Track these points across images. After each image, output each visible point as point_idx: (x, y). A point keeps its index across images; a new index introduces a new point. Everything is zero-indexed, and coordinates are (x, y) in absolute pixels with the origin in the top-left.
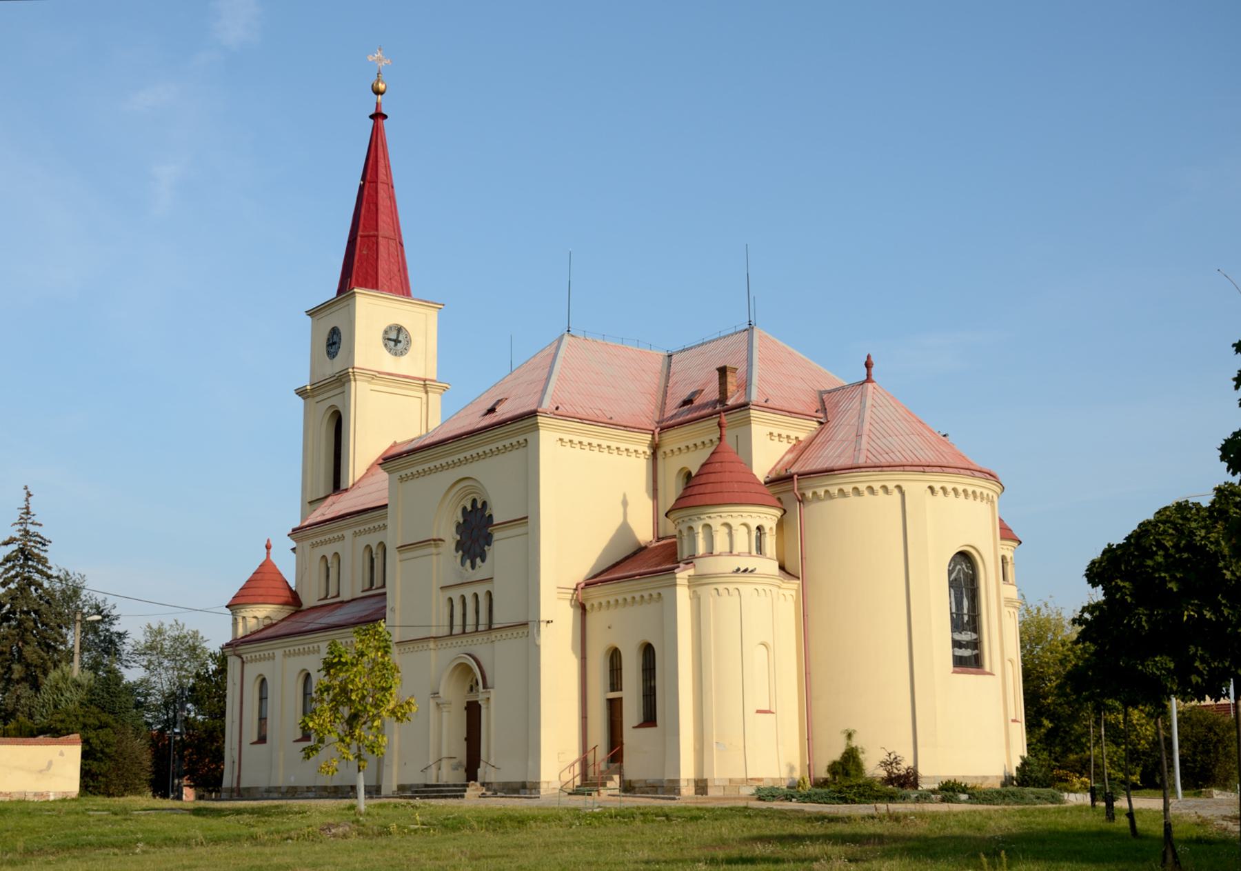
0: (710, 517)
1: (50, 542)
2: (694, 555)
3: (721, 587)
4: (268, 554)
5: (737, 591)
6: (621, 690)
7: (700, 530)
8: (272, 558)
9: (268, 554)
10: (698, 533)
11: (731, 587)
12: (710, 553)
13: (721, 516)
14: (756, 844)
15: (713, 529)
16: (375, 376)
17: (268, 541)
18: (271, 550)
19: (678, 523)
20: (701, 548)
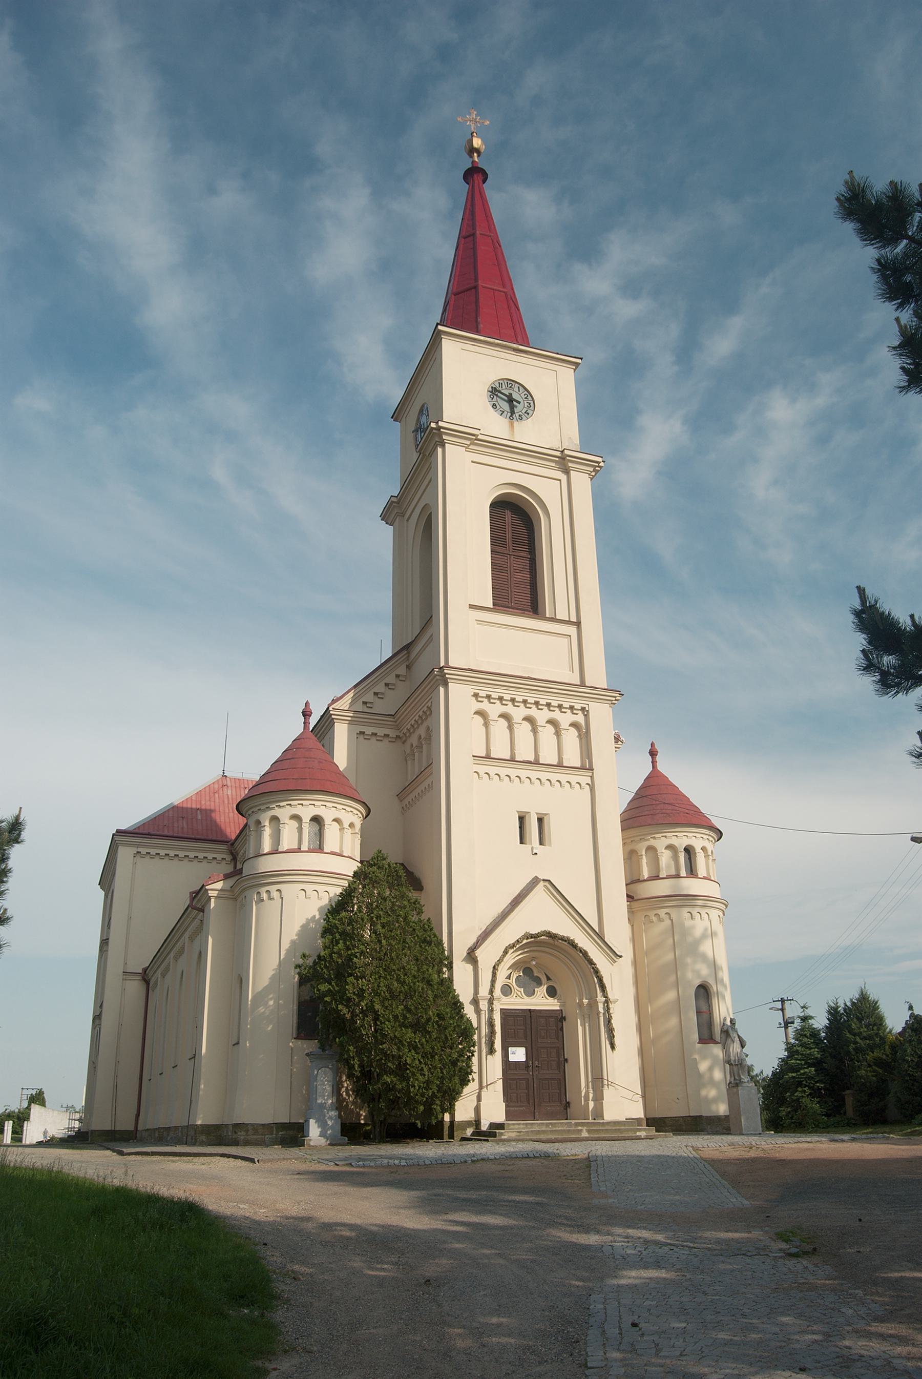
0: (654, 838)
1: (874, 299)
2: (658, 876)
3: (694, 912)
4: (654, 763)
5: (667, 916)
6: (501, 1009)
7: (267, 824)
8: (660, 767)
9: (654, 763)
10: (642, 855)
11: (703, 911)
12: (275, 852)
13: (666, 837)
14: (80, 1120)
15: (659, 851)
16: (472, 439)
17: (307, 704)
18: (658, 758)
19: (249, 815)
20: (267, 847)
